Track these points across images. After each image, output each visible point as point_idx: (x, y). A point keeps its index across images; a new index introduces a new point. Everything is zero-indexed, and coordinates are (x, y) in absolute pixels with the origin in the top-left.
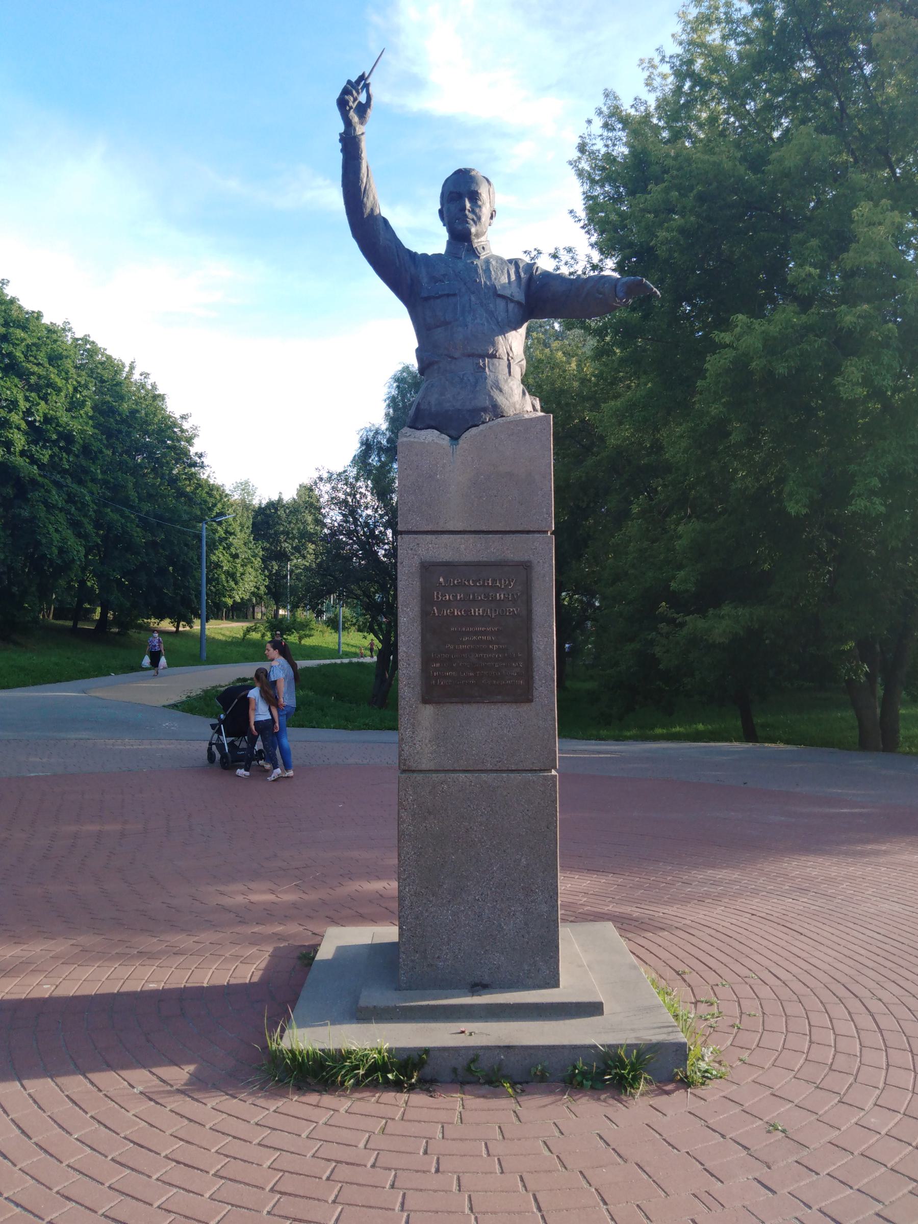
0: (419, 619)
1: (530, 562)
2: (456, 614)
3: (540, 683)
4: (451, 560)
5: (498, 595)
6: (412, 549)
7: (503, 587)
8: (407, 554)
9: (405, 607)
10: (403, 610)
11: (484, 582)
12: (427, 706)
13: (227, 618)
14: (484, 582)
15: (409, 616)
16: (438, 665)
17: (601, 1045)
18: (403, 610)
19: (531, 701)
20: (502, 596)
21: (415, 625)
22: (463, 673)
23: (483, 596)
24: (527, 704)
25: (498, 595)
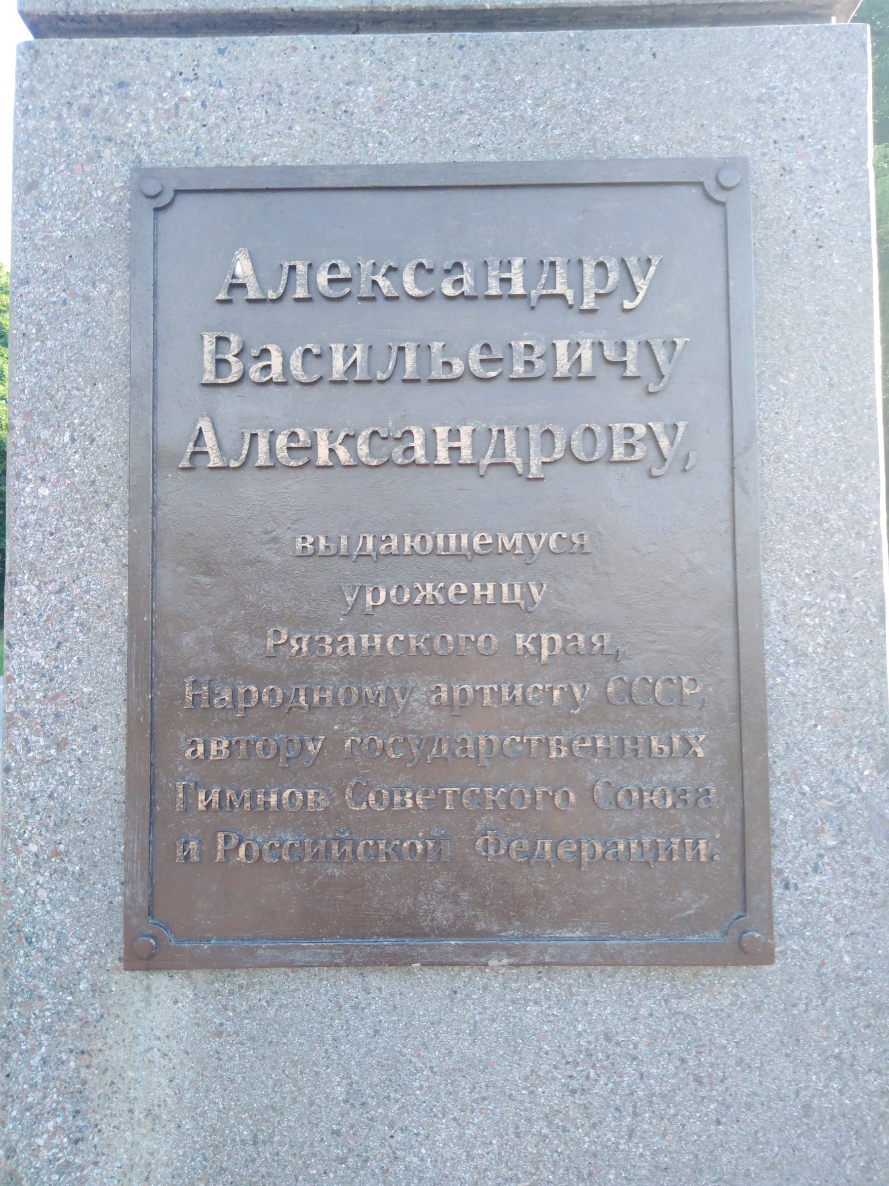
0: (122, 491)
1: (739, 163)
2: (323, 455)
3: (809, 851)
4: (302, 160)
5: (562, 347)
6: (86, 112)
7: (589, 302)
8: (64, 134)
9: (46, 422)
10: (32, 441)
11: (481, 278)
12: (160, 981)
13: (874, 122)
14: (481, 278)
15: (64, 472)
16: (219, 747)
17: (580, 357)
18: (32, 441)
19: (766, 956)
20: (586, 353)
21: (101, 520)
22: (359, 793)
23: (475, 355)
24: (735, 975)
25: (562, 347)
